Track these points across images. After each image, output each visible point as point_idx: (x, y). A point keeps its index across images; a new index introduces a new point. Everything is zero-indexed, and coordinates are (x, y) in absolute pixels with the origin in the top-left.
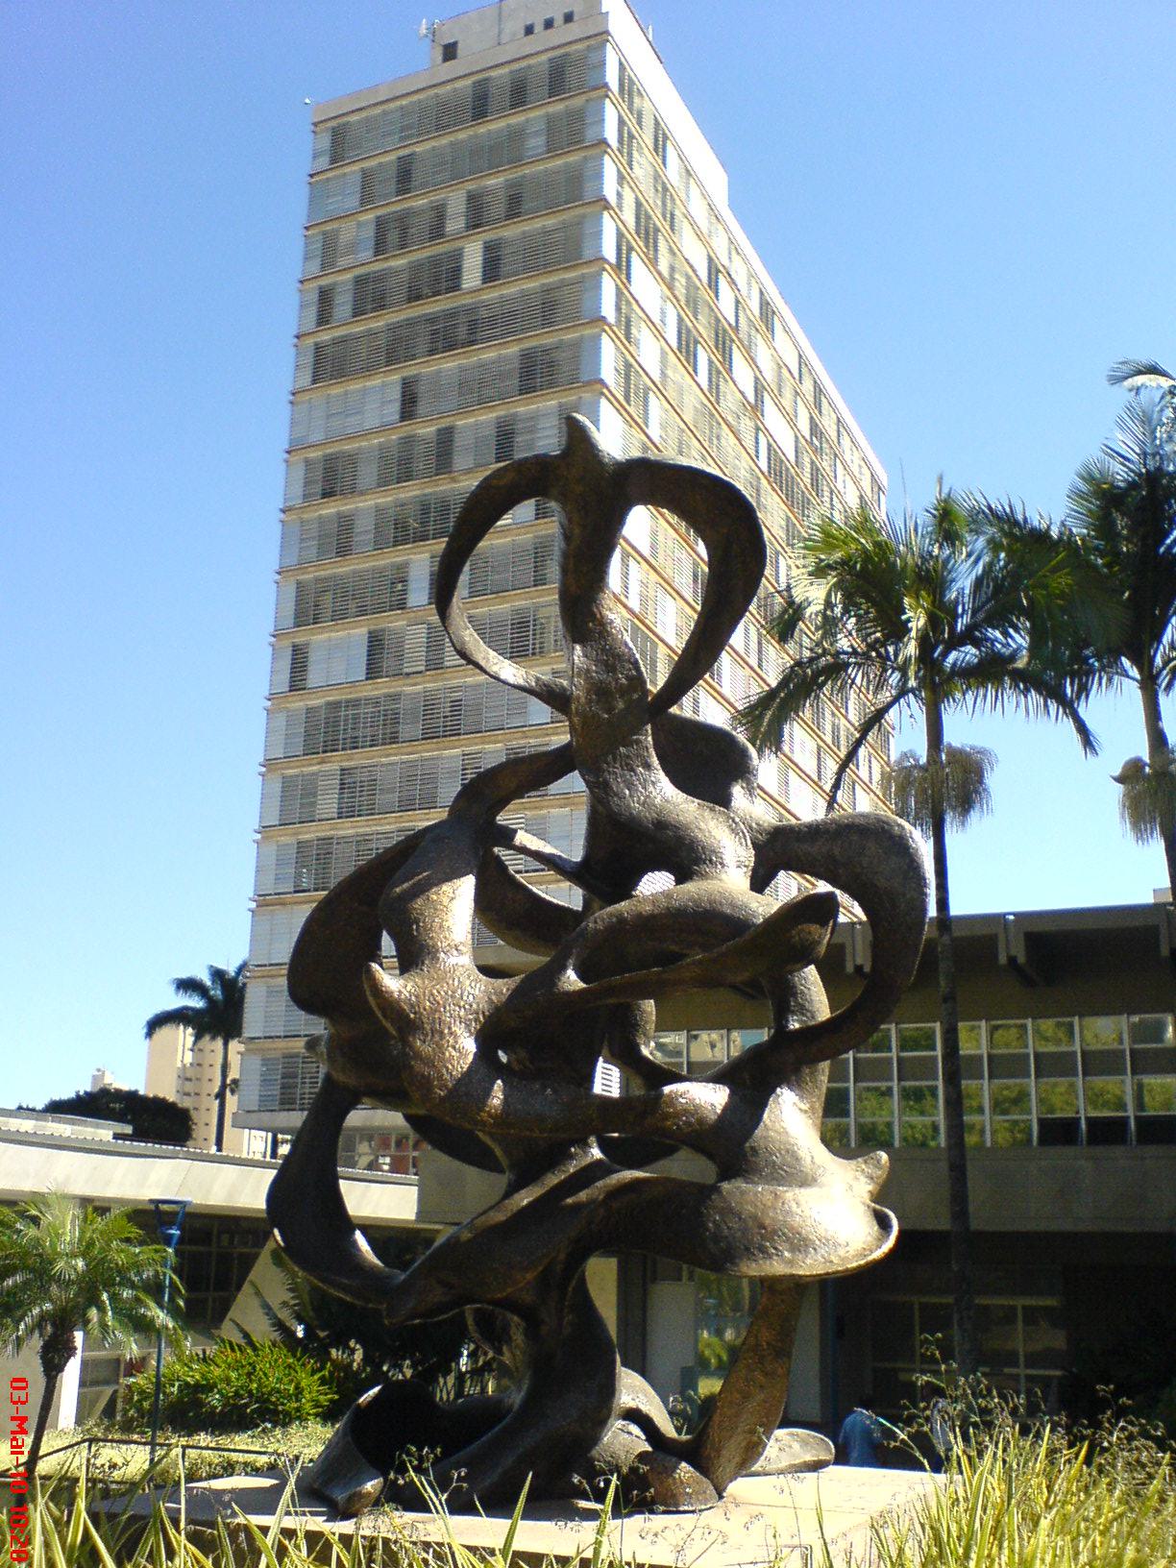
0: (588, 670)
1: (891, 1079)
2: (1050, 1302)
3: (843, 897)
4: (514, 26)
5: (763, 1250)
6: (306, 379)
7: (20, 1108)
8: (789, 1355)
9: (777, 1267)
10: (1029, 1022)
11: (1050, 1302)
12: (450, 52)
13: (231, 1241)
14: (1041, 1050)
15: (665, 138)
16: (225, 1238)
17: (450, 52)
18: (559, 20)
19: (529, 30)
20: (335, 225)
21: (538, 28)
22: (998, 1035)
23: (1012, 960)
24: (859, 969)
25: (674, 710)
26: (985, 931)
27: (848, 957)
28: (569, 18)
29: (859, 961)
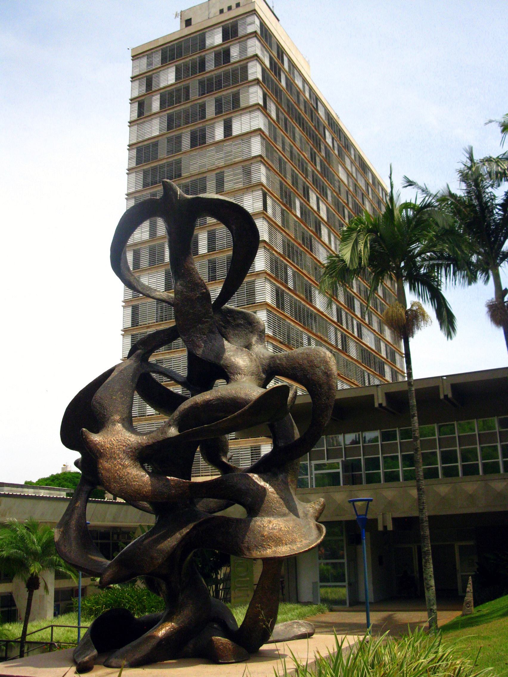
0: (182, 291)
1: (398, 452)
2: (471, 543)
3: (295, 385)
4: (215, 11)
5: (263, 546)
6: (134, 165)
7: (26, 483)
8: (313, 583)
9: (269, 552)
10: (455, 423)
11: (471, 543)
12: (188, 23)
13: (118, 538)
14: (461, 435)
15: (282, 53)
16: (115, 537)
17: (188, 23)
18: (234, 6)
19: (221, 11)
20: (143, 98)
21: (225, 10)
22: (442, 429)
23: (446, 396)
24: (380, 405)
25: (227, 305)
26: (432, 384)
27: (376, 401)
28: (238, 5)
29: (380, 402)
